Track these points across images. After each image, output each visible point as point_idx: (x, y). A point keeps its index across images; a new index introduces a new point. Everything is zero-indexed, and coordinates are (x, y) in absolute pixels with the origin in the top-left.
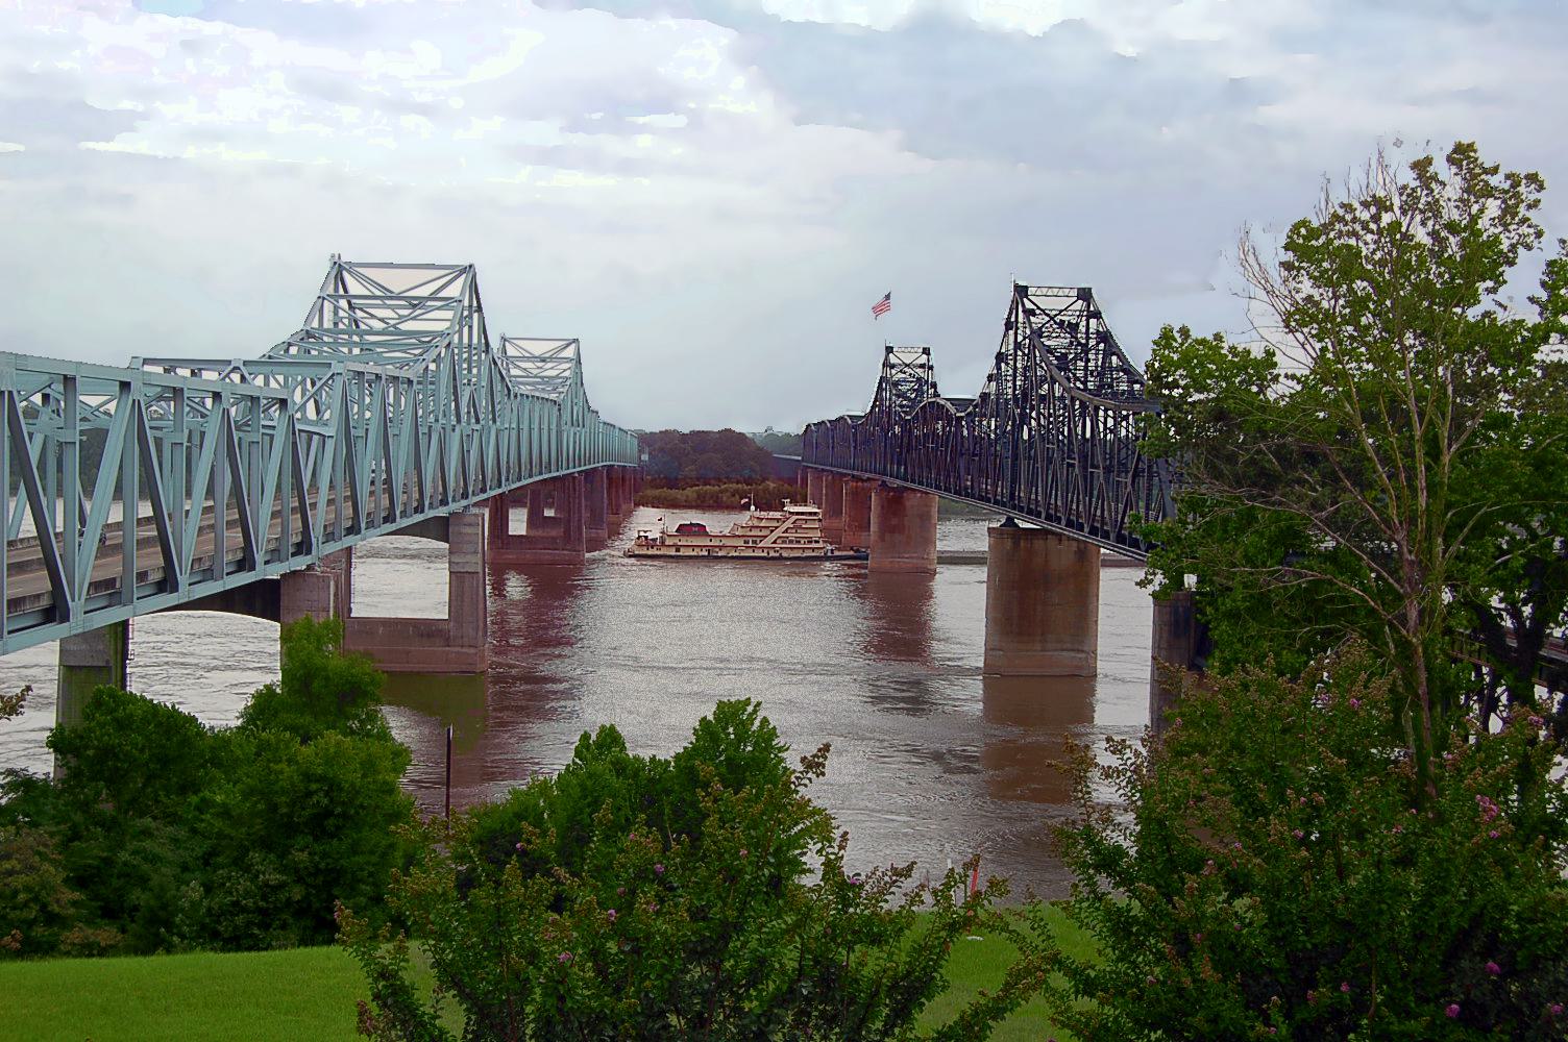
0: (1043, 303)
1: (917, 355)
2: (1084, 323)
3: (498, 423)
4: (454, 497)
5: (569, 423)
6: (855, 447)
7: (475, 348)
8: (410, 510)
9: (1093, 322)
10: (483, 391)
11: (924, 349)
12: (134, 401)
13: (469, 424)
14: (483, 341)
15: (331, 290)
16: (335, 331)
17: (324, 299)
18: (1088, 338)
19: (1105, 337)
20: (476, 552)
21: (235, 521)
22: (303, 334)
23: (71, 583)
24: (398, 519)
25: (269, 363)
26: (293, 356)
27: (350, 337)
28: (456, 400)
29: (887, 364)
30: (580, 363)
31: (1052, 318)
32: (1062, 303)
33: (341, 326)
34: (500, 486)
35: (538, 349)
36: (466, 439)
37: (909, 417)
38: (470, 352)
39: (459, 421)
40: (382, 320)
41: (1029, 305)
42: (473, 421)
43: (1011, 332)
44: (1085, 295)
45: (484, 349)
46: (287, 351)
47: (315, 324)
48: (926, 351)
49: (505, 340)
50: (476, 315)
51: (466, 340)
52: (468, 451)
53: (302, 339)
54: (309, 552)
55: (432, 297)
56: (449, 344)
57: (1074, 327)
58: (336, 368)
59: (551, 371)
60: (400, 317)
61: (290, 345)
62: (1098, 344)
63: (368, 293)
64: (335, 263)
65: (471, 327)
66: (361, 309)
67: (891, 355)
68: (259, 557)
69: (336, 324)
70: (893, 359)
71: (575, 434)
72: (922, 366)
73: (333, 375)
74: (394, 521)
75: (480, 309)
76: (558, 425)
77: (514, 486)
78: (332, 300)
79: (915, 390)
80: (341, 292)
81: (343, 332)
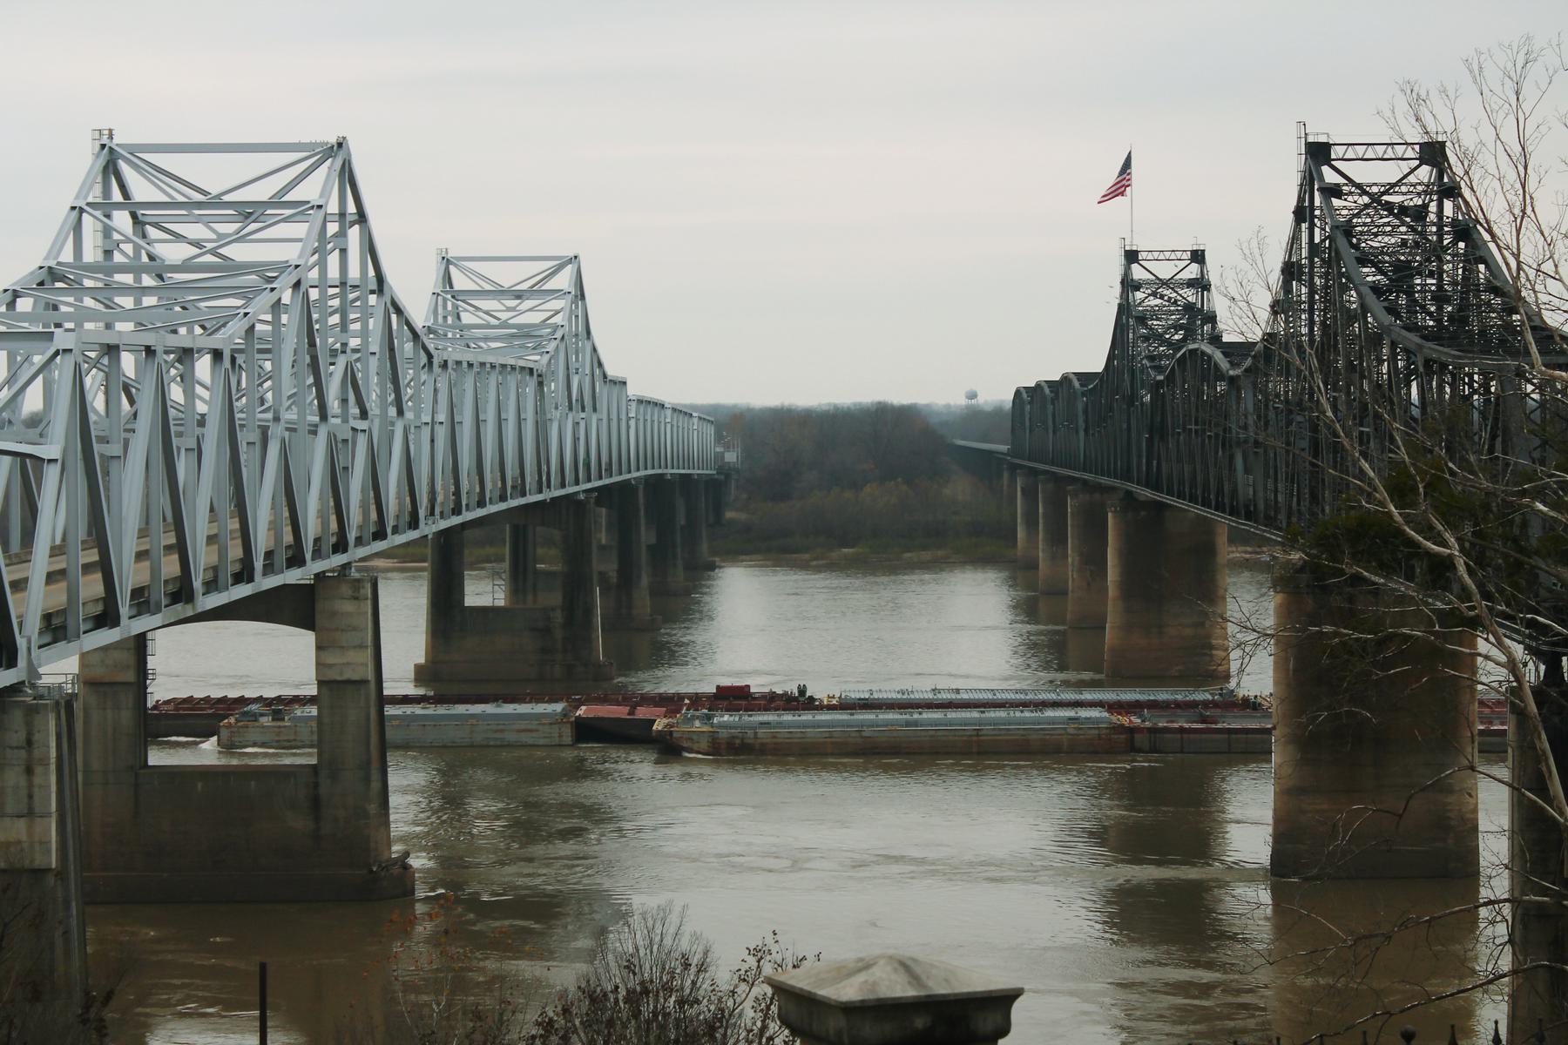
0: (1359, 172)
1: (1182, 264)
2: (1433, 207)
3: (409, 415)
4: (467, 505)
6: (1086, 431)
8: (367, 536)
9: (1448, 206)
10: (374, 363)
13: (345, 421)
14: (371, 273)
15: (95, 195)
17: (82, 210)
18: (1440, 234)
19: (1465, 231)
20: (362, 647)
22: (43, 274)
24: (124, 620)
26: (24, 317)
27: (138, 279)
28: (318, 383)
29: (1129, 285)
30: (583, 297)
31: (1375, 198)
32: (1390, 172)
33: (118, 258)
34: (540, 491)
35: (508, 276)
36: (336, 447)
37: (1161, 378)
38: (343, 296)
40: (178, 237)
41: (1330, 177)
42: (355, 411)
43: (1304, 226)
44: (1433, 153)
45: (374, 286)
46: (11, 305)
47: (67, 256)
48: (1198, 257)
50: (354, 233)
51: (333, 272)
53: (41, 284)
55: (276, 202)
57: (1420, 213)
58: (62, 340)
59: (531, 314)
60: (220, 236)
61: (16, 295)
62: (1454, 243)
63: (166, 199)
64: (103, 146)
65: (343, 251)
66: (156, 225)
67: (1135, 266)
69: (108, 253)
70: (1138, 273)
72: (1191, 283)
73: (57, 353)
74: (251, 579)
75: (362, 217)
76: (540, 410)
77: (444, 524)
79: (1181, 327)
80: (117, 196)
81: (123, 269)
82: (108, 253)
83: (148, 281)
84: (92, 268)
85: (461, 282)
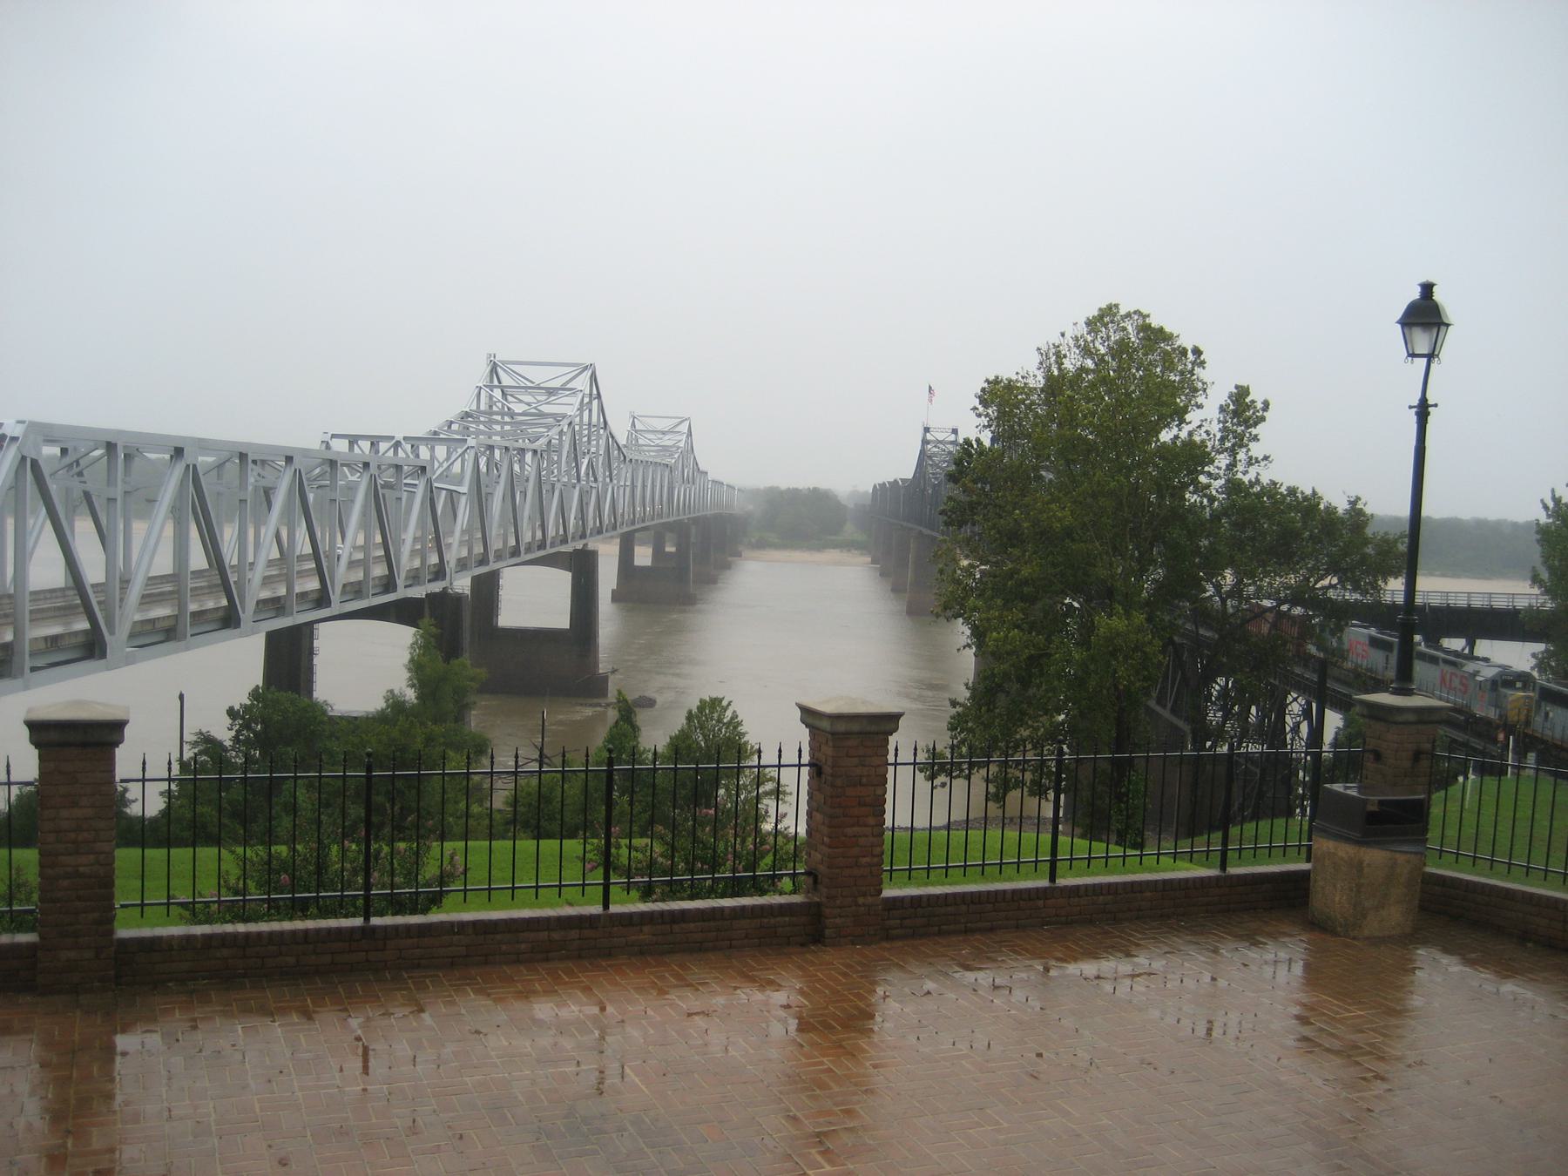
4: (591, 533)
5: (680, 481)
7: (594, 426)
10: (601, 458)
11: (953, 430)
12: (296, 470)
14: (602, 420)
16: (490, 412)
21: (216, 586)
23: (333, 586)
24: (548, 547)
25: (433, 439)
27: (503, 418)
29: (925, 442)
33: (495, 409)
38: (589, 429)
39: (579, 480)
45: (602, 426)
46: (450, 427)
49: (634, 417)
50: (595, 402)
52: (587, 504)
54: (444, 578)
56: (571, 423)
59: (667, 441)
60: (539, 401)
65: (590, 411)
66: (512, 395)
68: (400, 582)
69: (491, 407)
70: (929, 437)
71: (685, 491)
73: (468, 448)
78: (487, 390)
80: (496, 383)
81: (497, 413)
82: (491, 407)
83: (507, 419)
84: (484, 413)
85: (639, 426)
